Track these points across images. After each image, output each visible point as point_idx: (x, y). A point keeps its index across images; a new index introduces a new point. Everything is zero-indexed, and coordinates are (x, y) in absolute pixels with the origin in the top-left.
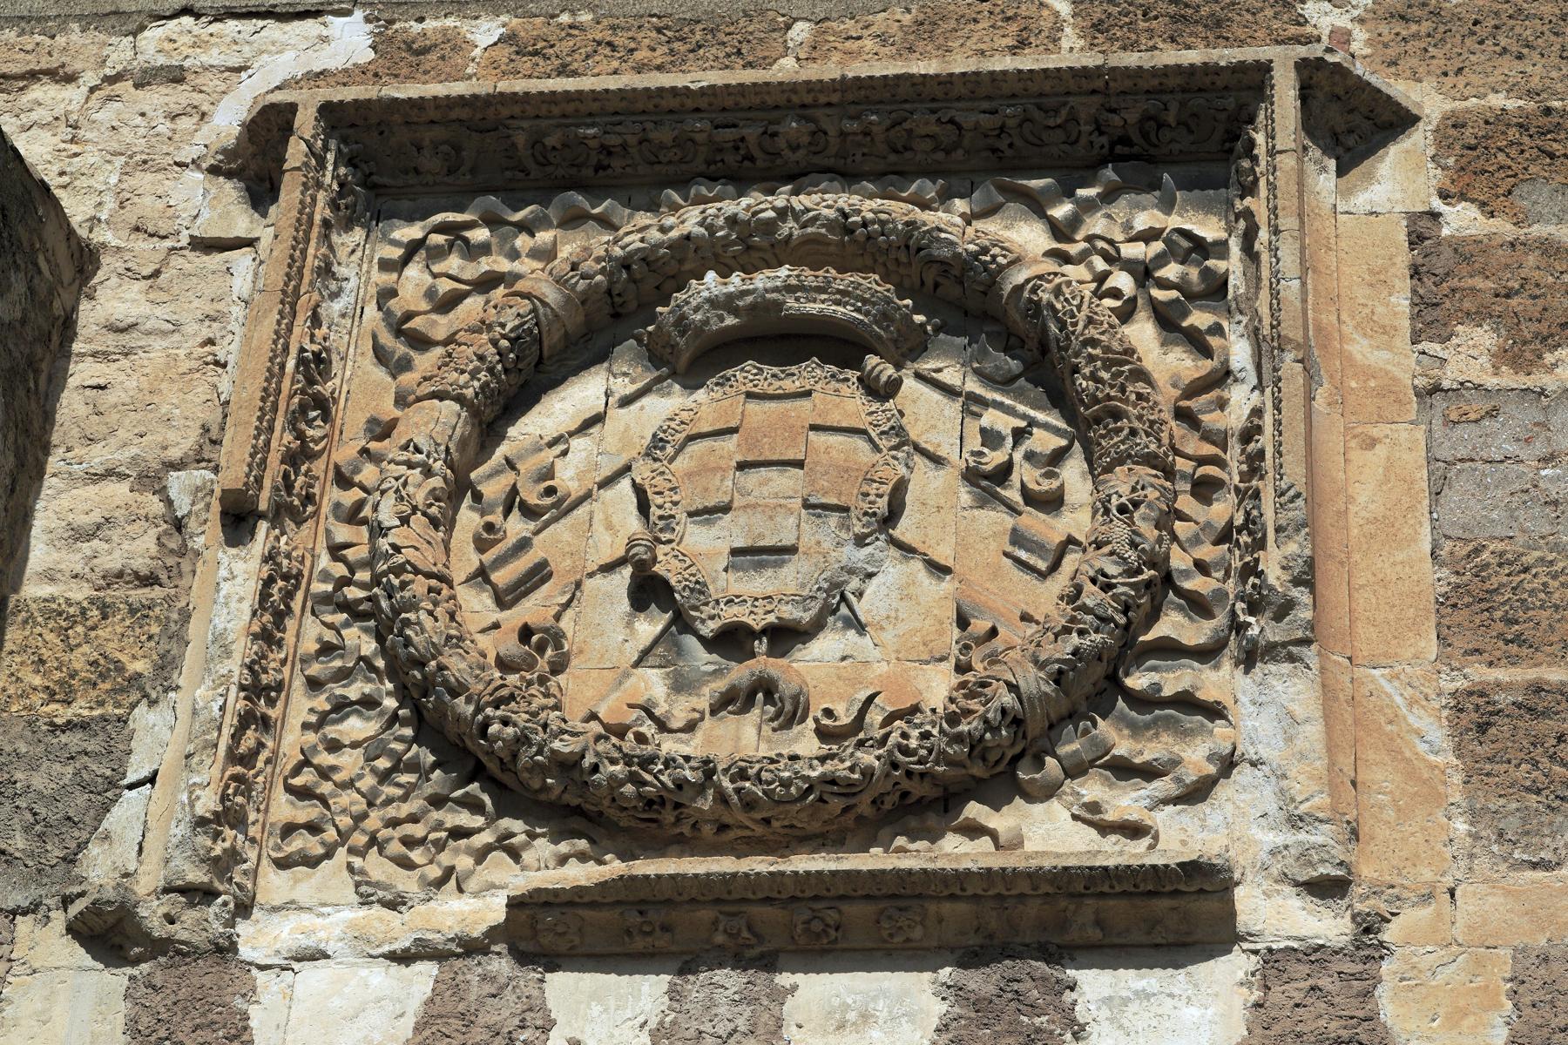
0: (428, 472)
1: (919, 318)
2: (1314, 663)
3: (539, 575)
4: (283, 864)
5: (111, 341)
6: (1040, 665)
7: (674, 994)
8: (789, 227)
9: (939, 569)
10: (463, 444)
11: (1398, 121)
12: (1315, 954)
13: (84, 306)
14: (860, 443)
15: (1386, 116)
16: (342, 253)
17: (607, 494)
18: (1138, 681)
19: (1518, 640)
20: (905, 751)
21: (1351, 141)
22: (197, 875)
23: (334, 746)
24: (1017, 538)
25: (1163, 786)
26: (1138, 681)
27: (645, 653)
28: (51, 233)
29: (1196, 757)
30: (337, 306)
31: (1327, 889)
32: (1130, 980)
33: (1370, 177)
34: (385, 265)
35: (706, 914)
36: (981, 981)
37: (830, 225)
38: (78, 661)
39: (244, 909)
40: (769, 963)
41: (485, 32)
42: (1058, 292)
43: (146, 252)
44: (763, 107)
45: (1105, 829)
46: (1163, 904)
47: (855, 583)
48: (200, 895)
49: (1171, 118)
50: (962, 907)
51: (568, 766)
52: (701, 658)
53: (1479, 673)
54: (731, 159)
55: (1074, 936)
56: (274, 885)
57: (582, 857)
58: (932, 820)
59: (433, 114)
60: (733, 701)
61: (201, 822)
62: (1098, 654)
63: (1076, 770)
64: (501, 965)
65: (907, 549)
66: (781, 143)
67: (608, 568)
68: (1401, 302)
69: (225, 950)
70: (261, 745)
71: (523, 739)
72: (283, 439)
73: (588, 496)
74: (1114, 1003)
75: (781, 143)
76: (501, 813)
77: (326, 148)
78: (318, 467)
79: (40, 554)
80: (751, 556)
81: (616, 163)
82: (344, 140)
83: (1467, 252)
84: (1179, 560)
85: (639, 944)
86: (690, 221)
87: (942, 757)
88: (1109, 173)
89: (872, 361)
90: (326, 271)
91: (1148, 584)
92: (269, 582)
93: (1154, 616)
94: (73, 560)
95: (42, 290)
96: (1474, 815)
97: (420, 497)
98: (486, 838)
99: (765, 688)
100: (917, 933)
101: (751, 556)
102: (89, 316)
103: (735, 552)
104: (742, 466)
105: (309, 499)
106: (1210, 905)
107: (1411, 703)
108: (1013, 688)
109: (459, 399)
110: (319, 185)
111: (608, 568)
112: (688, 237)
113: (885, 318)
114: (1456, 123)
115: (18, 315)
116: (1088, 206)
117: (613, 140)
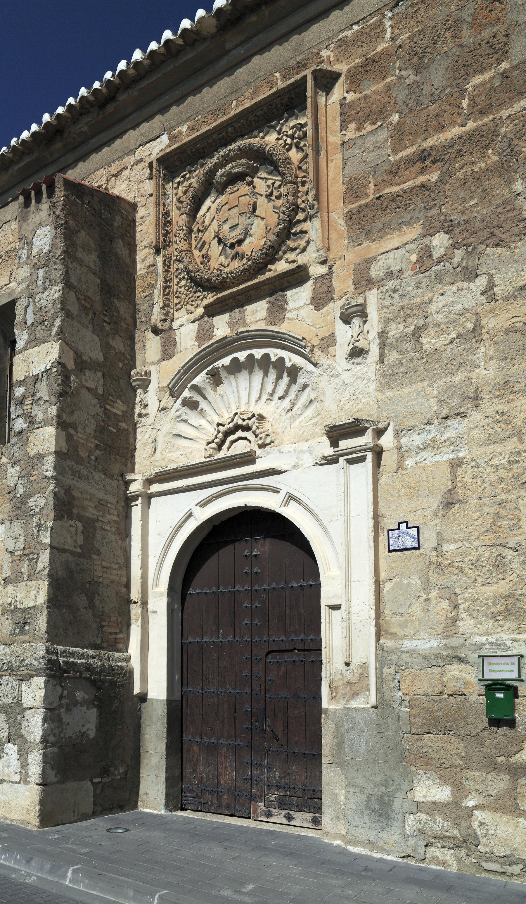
0: (183, 230)
1: (255, 164)
2: (319, 216)
3: (204, 243)
4: (177, 311)
5: (141, 221)
6: (274, 234)
7: (230, 316)
8: (232, 153)
9: (263, 219)
10: (189, 222)
11: (336, 76)
12: (323, 276)
13: (136, 215)
14: (247, 197)
15: (334, 76)
16: (168, 189)
17: (213, 223)
18: (293, 231)
19: (357, 197)
20: (255, 259)
21: (329, 86)
22: (163, 317)
23: (180, 287)
24: (274, 207)
25: (298, 251)
26: (293, 231)
27: (221, 253)
28: (123, 205)
29: (303, 243)
30: (169, 201)
31: (323, 262)
32: (295, 291)
33: (333, 94)
34: (175, 188)
35: (231, 300)
36: (272, 299)
37: (238, 150)
38: (146, 284)
39: (172, 320)
40: (242, 306)
41: (184, 128)
42: (274, 150)
43: (144, 199)
44: (224, 127)
45: (290, 263)
46: (296, 275)
47: (250, 227)
48: (164, 320)
49: (293, 96)
50: (267, 286)
51: (208, 280)
52: (229, 250)
53: (351, 206)
54: (223, 141)
55: (285, 286)
56: (176, 315)
57: (215, 295)
58: (264, 271)
59: (174, 153)
60: (233, 258)
61: (161, 308)
62: (284, 228)
63: (285, 253)
64: (206, 319)
65: (258, 216)
66: (229, 134)
67: (214, 238)
68: (338, 124)
69: (171, 328)
70: (169, 291)
71: (201, 278)
72: (162, 232)
73: (210, 224)
74: (292, 296)
75: (229, 134)
76: (204, 291)
77: (160, 168)
78: (171, 235)
79: (139, 266)
80: (233, 228)
81: (205, 150)
82: (163, 165)
83: (351, 105)
84: (299, 201)
85: (224, 308)
86: (215, 160)
87: (261, 259)
88: (286, 115)
89: (247, 178)
90: (165, 194)
91: (293, 210)
92: (165, 261)
93: (297, 214)
94: (143, 266)
95: (125, 216)
96: (349, 238)
97: (182, 236)
98: (202, 297)
99: (237, 253)
100: (262, 293)
101: (233, 228)
102: (138, 217)
103: (230, 228)
104: (229, 209)
105: (170, 242)
106: (303, 273)
107: (339, 218)
108: (270, 241)
109: (185, 213)
110: (160, 177)
111: (214, 238)
112: (215, 163)
113: (248, 168)
114: (349, 71)
115: (120, 223)
116: (283, 125)
117: (203, 146)
